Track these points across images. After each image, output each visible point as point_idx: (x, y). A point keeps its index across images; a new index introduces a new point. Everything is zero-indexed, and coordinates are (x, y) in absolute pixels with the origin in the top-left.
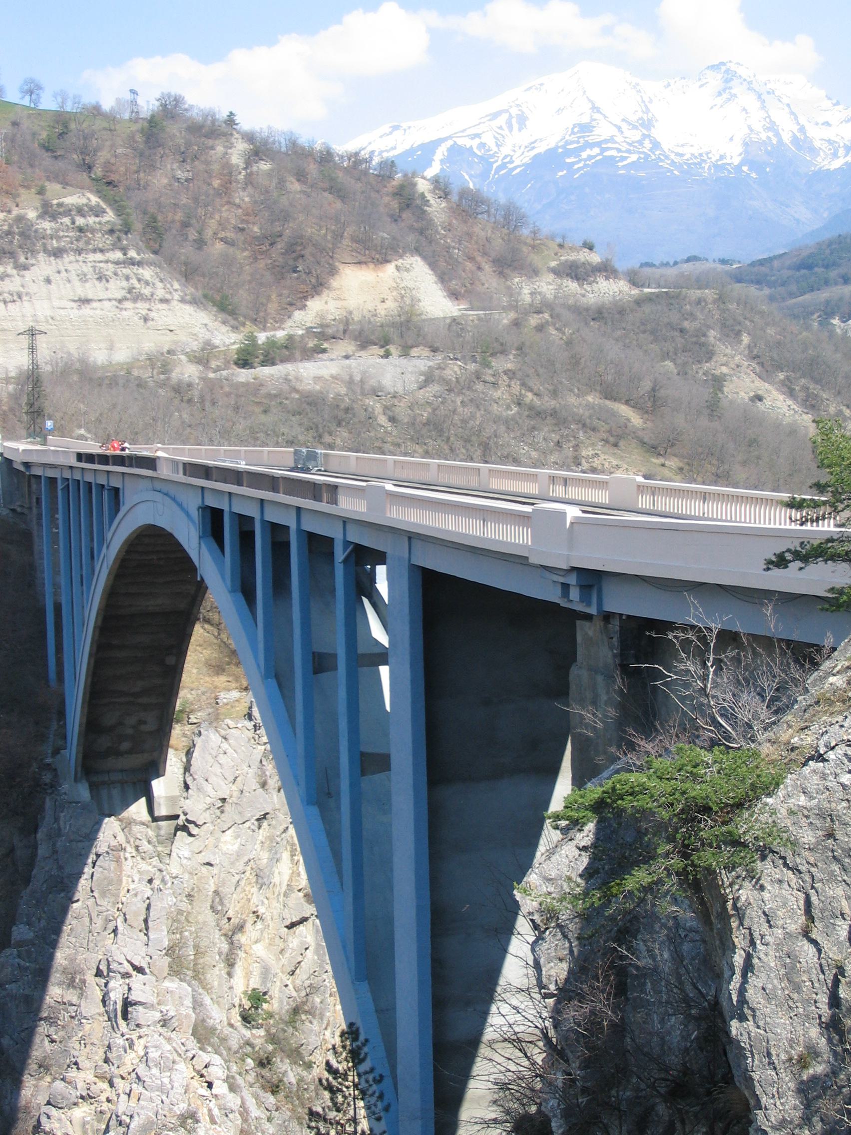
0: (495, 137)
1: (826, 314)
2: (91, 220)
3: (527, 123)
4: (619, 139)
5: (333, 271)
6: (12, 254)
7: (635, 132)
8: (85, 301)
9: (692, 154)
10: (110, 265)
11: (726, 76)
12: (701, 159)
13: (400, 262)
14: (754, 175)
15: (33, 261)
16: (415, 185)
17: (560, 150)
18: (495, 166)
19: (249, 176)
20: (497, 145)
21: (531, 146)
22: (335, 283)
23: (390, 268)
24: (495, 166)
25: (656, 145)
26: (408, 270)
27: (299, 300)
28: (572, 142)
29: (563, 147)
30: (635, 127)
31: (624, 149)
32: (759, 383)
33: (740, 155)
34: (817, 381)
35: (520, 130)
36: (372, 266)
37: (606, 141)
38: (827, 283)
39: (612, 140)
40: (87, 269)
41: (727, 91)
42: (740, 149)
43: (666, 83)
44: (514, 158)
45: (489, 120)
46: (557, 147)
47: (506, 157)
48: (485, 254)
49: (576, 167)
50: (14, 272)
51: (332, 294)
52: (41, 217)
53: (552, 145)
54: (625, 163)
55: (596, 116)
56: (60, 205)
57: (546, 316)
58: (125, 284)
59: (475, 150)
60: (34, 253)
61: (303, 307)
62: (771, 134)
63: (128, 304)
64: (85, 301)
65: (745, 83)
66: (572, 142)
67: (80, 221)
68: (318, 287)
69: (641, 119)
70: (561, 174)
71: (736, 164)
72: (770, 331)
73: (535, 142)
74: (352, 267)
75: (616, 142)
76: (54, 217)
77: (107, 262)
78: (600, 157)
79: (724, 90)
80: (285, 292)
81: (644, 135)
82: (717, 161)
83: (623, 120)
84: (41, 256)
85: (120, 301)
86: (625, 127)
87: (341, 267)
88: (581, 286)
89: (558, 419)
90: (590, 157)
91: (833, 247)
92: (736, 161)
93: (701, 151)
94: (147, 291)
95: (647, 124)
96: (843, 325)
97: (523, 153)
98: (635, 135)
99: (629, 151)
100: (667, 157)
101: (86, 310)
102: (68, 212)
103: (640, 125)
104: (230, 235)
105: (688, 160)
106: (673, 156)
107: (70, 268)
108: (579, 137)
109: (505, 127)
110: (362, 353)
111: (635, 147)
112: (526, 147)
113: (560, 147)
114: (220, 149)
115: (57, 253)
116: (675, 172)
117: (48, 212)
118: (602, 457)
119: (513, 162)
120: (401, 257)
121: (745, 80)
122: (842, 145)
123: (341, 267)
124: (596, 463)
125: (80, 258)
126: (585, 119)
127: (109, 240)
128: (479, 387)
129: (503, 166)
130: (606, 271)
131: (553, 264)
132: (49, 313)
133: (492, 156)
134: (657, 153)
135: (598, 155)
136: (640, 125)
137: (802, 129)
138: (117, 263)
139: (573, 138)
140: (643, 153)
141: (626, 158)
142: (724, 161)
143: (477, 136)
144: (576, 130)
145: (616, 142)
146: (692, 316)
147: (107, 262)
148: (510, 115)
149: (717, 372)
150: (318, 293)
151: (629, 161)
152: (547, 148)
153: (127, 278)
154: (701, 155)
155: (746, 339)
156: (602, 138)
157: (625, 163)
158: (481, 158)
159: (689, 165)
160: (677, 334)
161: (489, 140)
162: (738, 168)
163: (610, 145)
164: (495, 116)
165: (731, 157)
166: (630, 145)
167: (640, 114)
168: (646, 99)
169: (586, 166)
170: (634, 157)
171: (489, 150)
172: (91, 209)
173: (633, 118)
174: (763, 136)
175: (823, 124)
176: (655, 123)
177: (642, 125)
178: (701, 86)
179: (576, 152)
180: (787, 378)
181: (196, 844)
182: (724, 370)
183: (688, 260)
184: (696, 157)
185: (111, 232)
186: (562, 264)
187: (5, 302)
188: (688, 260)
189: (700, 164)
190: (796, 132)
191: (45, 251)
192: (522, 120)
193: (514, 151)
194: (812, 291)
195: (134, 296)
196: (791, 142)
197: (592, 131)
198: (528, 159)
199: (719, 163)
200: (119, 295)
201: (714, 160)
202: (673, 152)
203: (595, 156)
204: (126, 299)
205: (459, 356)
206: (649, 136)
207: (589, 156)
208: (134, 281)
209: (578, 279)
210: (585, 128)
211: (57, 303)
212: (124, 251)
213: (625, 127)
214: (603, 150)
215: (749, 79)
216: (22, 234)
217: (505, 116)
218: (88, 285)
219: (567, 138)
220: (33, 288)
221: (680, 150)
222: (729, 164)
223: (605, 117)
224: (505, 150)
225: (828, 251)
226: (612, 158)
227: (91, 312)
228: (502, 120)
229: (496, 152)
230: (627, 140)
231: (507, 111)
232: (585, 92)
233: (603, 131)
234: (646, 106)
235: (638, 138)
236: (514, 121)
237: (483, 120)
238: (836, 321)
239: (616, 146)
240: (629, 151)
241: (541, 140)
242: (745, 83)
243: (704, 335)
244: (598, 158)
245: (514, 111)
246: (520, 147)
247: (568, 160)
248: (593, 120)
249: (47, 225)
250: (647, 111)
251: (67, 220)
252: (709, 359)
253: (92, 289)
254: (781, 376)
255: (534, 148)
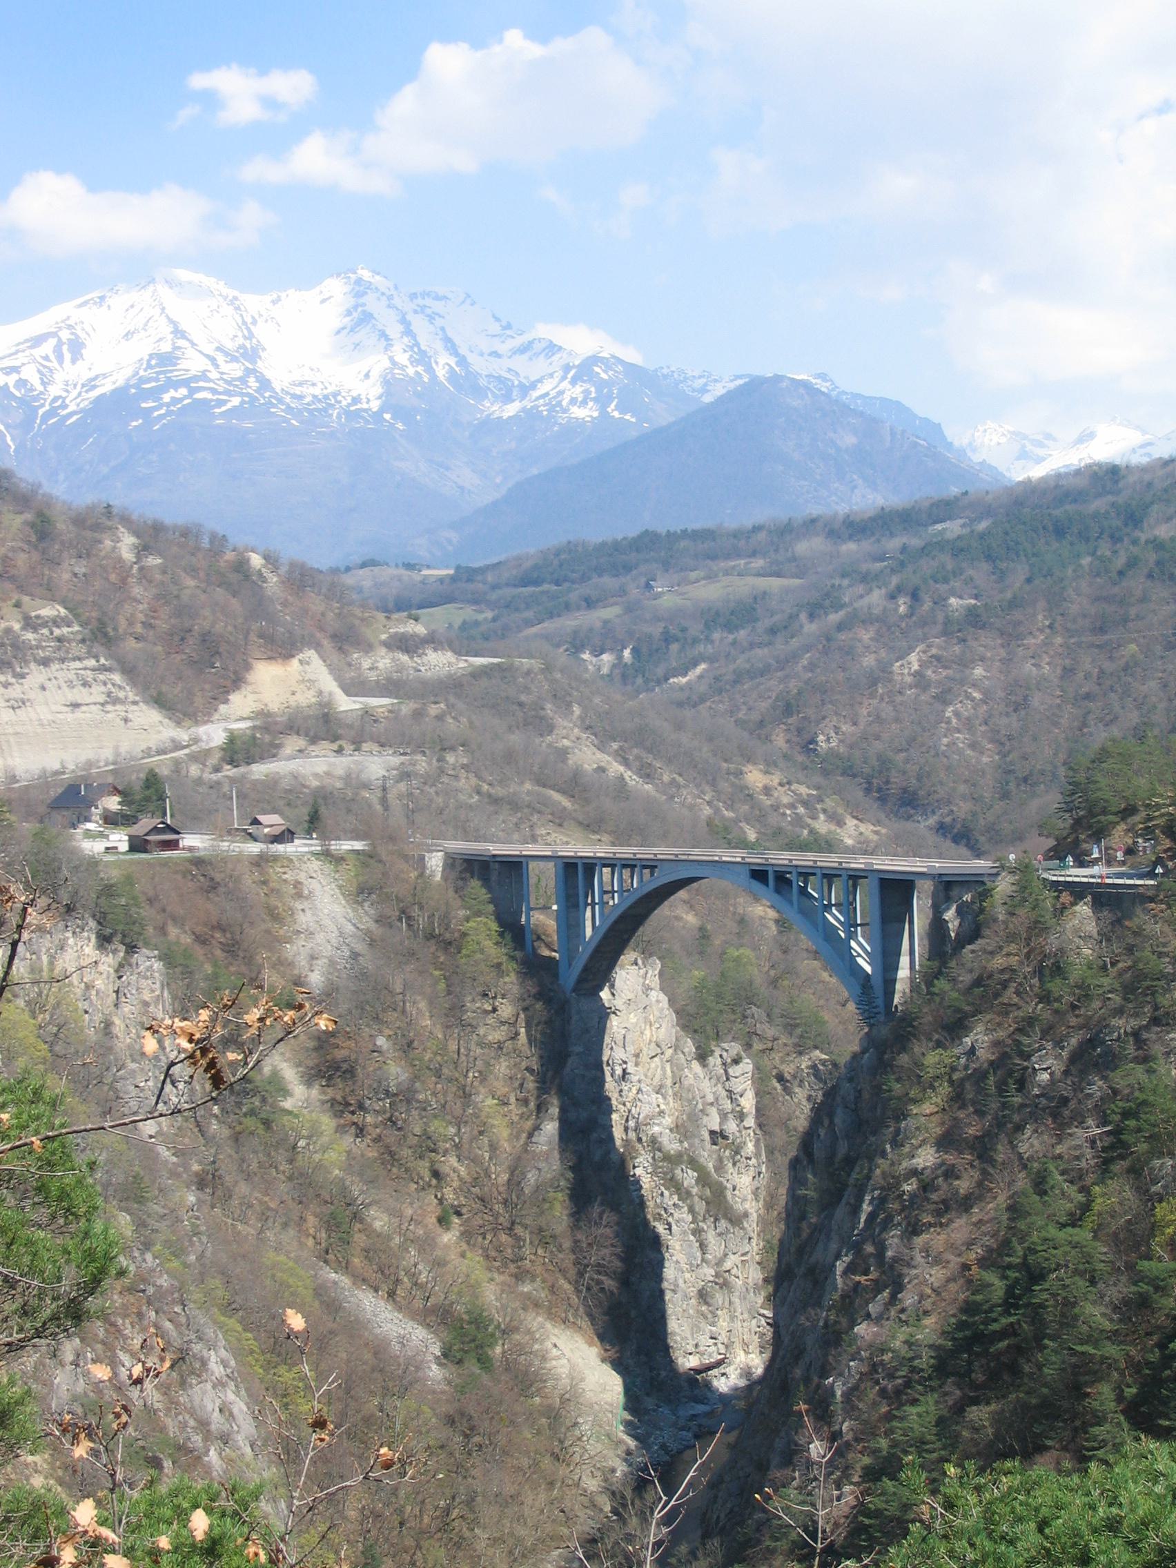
0: (39, 371)
1: (574, 647)
2: (65, 630)
3: (83, 351)
4: (214, 375)
5: (248, 667)
6: (9, 665)
7: (235, 365)
8: (75, 706)
9: (314, 396)
10: (89, 672)
11: (357, 288)
12: (327, 401)
13: (301, 656)
14: (400, 426)
15: (26, 671)
16: (248, 560)
17: (133, 391)
18: (41, 412)
19: (141, 569)
20: (43, 383)
21: (90, 385)
22: (251, 677)
23: (295, 662)
24: (41, 412)
25: (265, 384)
26: (308, 663)
27: (222, 693)
28: (149, 380)
29: (137, 386)
30: (234, 359)
31: (221, 390)
32: (599, 755)
33: (380, 398)
34: (650, 751)
35: (74, 361)
36: (280, 661)
37: (196, 378)
38: (567, 607)
39: (203, 376)
40: (71, 676)
41: (360, 309)
42: (379, 390)
43: (275, 296)
44: (67, 401)
45: (30, 347)
46: (127, 387)
47: (56, 399)
48: (322, 629)
49: (156, 414)
50: (13, 680)
51: (249, 688)
52: (23, 628)
53: (121, 382)
54: (224, 409)
55: (181, 343)
56: (38, 617)
57: (442, 706)
58: (103, 689)
59: (12, 389)
60: (27, 662)
61: (226, 701)
62: (420, 369)
63: (109, 707)
64: (75, 706)
65: (384, 298)
66: (149, 380)
67: (57, 632)
68: (237, 682)
69: (243, 346)
70: (134, 424)
71: (375, 410)
72: (597, 700)
73: (96, 377)
74: (263, 662)
75: (210, 380)
76: (35, 629)
77: (85, 669)
78: (189, 401)
79: (356, 307)
80: (207, 687)
81: (247, 369)
82: (349, 405)
83: (218, 349)
84: (33, 665)
85: (102, 705)
86: (220, 358)
87: (254, 662)
88: (411, 658)
89: (514, 804)
90: (175, 401)
91: (563, 557)
92: (375, 405)
93: (325, 392)
94: (121, 695)
95: (250, 354)
96: (594, 660)
97: (80, 394)
98: (235, 370)
99: (227, 393)
100: (281, 401)
101: (79, 714)
102: (45, 624)
103: (242, 355)
104: (139, 629)
105: (308, 404)
106: (288, 399)
107: (56, 674)
108: (158, 373)
109: (52, 357)
110: (312, 748)
111: (236, 386)
112: (83, 386)
113: (132, 386)
114: (108, 543)
115: (45, 662)
116: (294, 422)
117: (30, 623)
118: (554, 835)
119: (66, 407)
120: (301, 651)
121: (383, 294)
122: (516, 383)
123: (254, 662)
124: (549, 839)
125: (64, 666)
126: (166, 347)
127: (83, 649)
128: (445, 779)
129: (52, 412)
130: (433, 642)
131: (384, 637)
132: (50, 717)
133: (36, 398)
134: (267, 394)
135: (185, 397)
136: (242, 355)
137: (462, 361)
138: (93, 670)
139: (150, 373)
140: (248, 394)
141: (225, 402)
142: (359, 406)
143: (15, 369)
144: (153, 362)
145: (210, 380)
146: (526, 689)
147: (85, 669)
148: (60, 340)
149: (559, 745)
150: (238, 688)
151: (229, 406)
152: (113, 387)
153: (105, 684)
154: (326, 397)
155: (577, 710)
156: (193, 373)
157: (224, 409)
158: (21, 401)
159: (311, 412)
160: (515, 707)
161: (30, 374)
162: (378, 416)
163: (201, 384)
164: (38, 341)
165: (368, 401)
166: (228, 382)
167: (240, 341)
168: (249, 320)
169: (169, 413)
170: (236, 401)
171: (32, 390)
172: (63, 619)
173: (230, 345)
174: (411, 371)
175: (490, 354)
176: (262, 354)
177: (244, 355)
178: (323, 301)
179: (155, 393)
180: (621, 748)
181: (620, 1020)
182: (566, 742)
183: (364, 565)
184: (320, 401)
185: (83, 641)
186: (391, 637)
187: (13, 708)
188: (364, 565)
189: (325, 410)
190: (454, 365)
191: (35, 661)
192: (77, 348)
193: (67, 391)
194: (551, 617)
195: (112, 700)
196: (448, 380)
197: (176, 365)
198: (86, 403)
199: (352, 408)
200: (102, 698)
201: (344, 403)
202: (287, 393)
203: (181, 400)
204: (107, 702)
205: (408, 751)
206: (254, 371)
207: (173, 398)
208: (110, 686)
209: (408, 652)
210: (166, 360)
211: (54, 708)
212: (97, 658)
213: (220, 358)
214: (193, 391)
215: (388, 293)
216: (12, 646)
217: (52, 342)
218: (75, 690)
219: (142, 373)
220: (32, 695)
221: (298, 391)
222: (365, 410)
223: (193, 344)
224: (54, 390)
225: (556, 562)
226: (205, 402)
227: (82, 715)
228: (48, 348)
229: (41, 393)
230: (225, 377)
231: (54, 335)
232: (163, 309)
233: (192, 364)
234: (248, 329)
235: (239, 374)
236: (65, 348)
237: (22, 347)
238: (586, 656)
239: (211, 385)
240: (227, 393)
241: (105, 376)
242: (384, 298)
243: (543, 709)
244: (186, 402)
245: (65, 335)
246: (75, 386)
247: (144, 405)
248: (176, 348)
249: (30, 636)
250: (250, 336)
251: (45, 631)
252: (550, 732)
253: (80, 694)
254: (615, 746)
255: (94, 387)
